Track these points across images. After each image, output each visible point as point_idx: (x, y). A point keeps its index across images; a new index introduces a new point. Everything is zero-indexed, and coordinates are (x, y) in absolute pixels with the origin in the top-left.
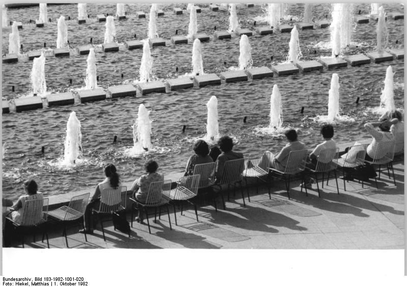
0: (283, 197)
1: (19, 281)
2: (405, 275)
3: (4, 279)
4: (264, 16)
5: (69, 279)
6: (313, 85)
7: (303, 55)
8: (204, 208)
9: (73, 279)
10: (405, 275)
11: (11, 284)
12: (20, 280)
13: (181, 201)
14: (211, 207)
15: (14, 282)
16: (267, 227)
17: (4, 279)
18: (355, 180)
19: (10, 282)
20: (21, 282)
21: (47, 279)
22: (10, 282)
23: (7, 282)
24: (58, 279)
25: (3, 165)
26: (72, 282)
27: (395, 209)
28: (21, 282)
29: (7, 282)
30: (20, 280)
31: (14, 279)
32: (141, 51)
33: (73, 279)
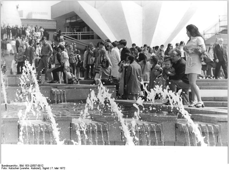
0: (83, 85)
1: (11, 167)
2: (228, 163)
3: (2, 165)
4: (124, 117)
5: (39, 166)
7: (125, 67)
9: (41, 166)
10: (228, 163)
11: (6, 169)
12: (11, 166)
13: (187, 110)
15: (8, 167)
16: (19, 67)
17: (2, 165)
19: (5, 167)
20: (15, 167)
22: (5, 167)
23: (4, 167)
25: (1, 61)
27: (124, 134)
28: (15, 167)
30: (11, 166)
31: (8, 166)
33: (41, 166)
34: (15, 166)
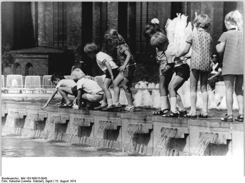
2: (244, 176)
3: (2, 178)
5: (42, 178)
6: (226, 115)
8: (34, 29)
9: (37, 178)
10: (244, 176)
12: (12, 179)
14: (73, 67)
15: (8, 180)
17: (2, 178)
18: (95, 108)
19: (6, 180)
21: (28, 178)
22: (6, 180)
23: (4, 180)
24: (33, 178)
26: (29, 180)
29: (4, 180)
30: (12, 179)
31: (9, 178)
32: (238, 4)
33: (37, 178)
34: (16, 179)
